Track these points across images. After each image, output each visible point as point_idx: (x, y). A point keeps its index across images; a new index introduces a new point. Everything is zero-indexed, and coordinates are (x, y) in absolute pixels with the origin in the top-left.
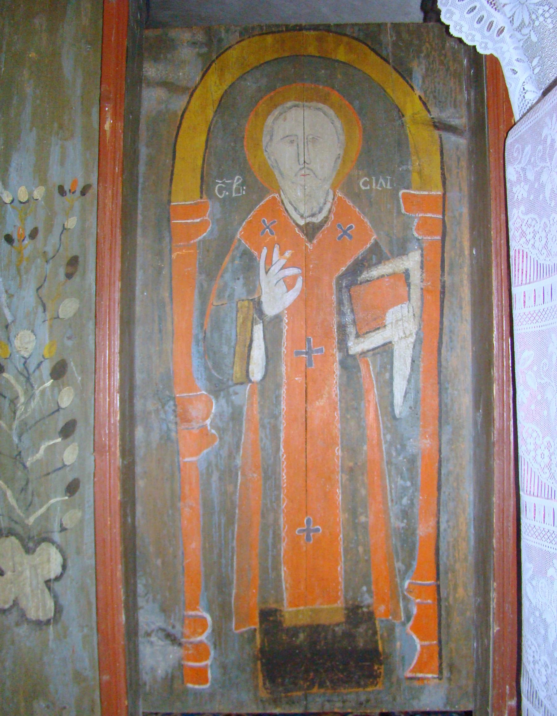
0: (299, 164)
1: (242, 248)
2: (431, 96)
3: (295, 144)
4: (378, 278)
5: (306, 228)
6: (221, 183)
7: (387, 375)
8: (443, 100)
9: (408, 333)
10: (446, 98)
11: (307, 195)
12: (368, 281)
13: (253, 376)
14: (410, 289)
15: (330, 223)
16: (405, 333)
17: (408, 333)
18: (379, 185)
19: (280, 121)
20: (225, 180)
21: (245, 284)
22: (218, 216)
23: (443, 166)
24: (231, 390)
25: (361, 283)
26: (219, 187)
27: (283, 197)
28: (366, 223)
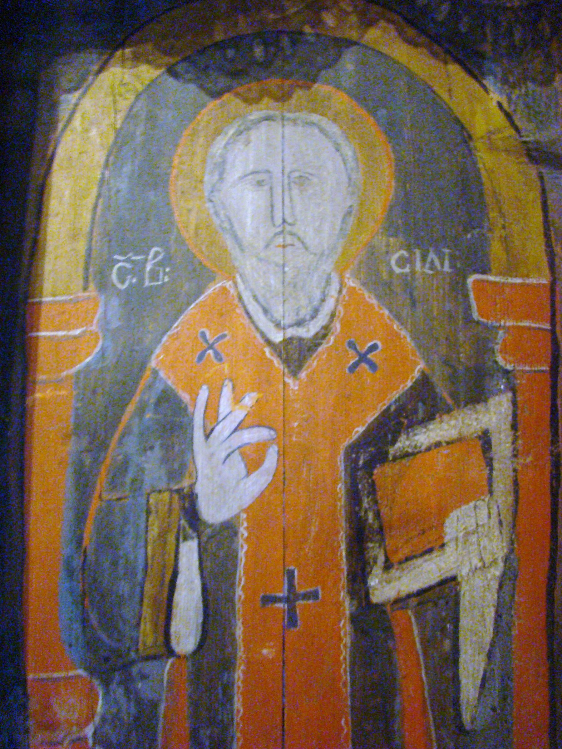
0: (274, 225)
1: (159, 387)
2: (520, 102)
3: (266, 188)
4: (428, 449)
5: (285, 349)
6: (124, 261)
7: (447, 644)
8: (543, 109)
9: (488, 559)
10: (548, 106)
11: (289, 284)
12: (407, 455)
13: (178, 643)
14: (491, 469)
15: (332, 339)
16: (482, 559)
17: (488, 559)
18: (428, 265)
19: (240, 146)
20: (130, 255)
21: (165, 460)
22: (115, 324)
23: (549, 230)
24: (135, 670)
25: (395, 459)
26: (120, 269)
27: (241, 287)
28: (404, 338)
